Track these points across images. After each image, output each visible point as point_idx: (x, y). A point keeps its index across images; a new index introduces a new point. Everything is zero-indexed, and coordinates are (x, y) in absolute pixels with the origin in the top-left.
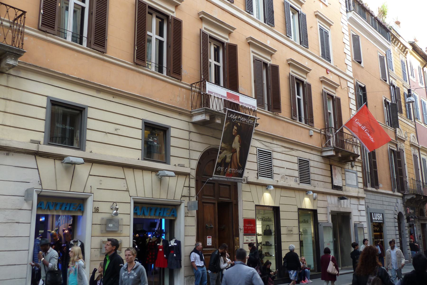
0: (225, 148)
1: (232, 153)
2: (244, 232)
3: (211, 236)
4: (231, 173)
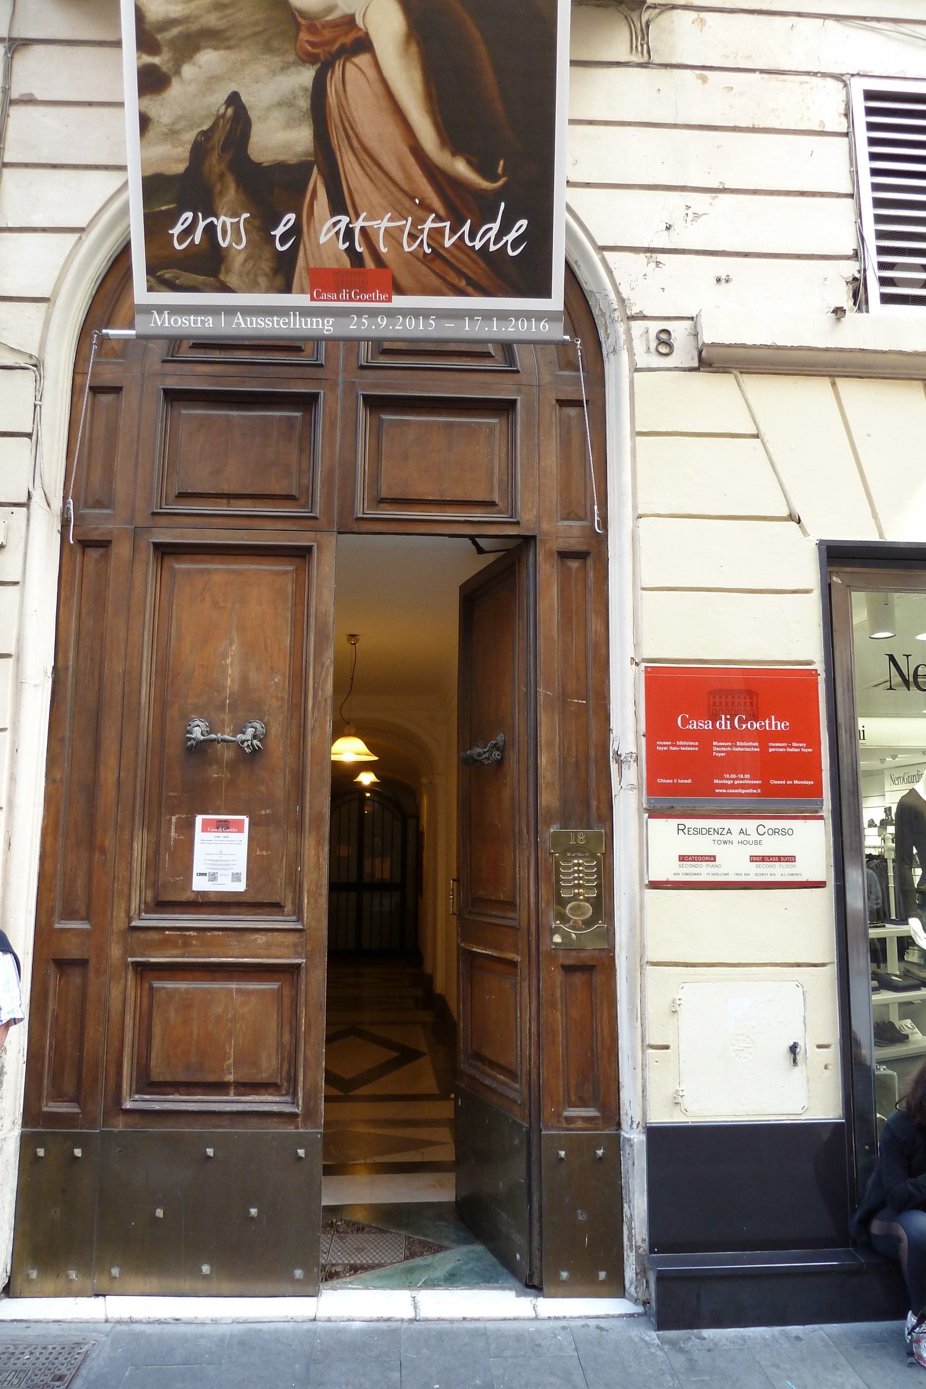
0: (195, 27)
1: (308, 59)
2: (653, 789)
3: (246, 820)
4: (370, 264)
